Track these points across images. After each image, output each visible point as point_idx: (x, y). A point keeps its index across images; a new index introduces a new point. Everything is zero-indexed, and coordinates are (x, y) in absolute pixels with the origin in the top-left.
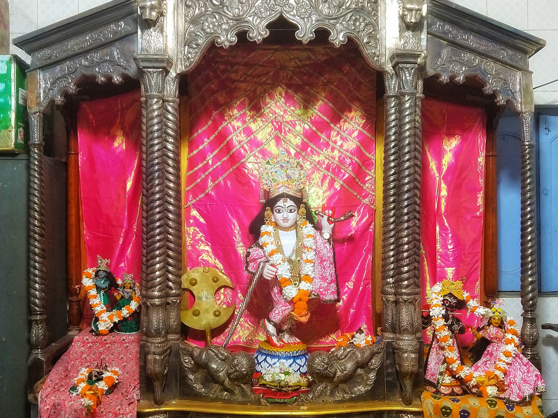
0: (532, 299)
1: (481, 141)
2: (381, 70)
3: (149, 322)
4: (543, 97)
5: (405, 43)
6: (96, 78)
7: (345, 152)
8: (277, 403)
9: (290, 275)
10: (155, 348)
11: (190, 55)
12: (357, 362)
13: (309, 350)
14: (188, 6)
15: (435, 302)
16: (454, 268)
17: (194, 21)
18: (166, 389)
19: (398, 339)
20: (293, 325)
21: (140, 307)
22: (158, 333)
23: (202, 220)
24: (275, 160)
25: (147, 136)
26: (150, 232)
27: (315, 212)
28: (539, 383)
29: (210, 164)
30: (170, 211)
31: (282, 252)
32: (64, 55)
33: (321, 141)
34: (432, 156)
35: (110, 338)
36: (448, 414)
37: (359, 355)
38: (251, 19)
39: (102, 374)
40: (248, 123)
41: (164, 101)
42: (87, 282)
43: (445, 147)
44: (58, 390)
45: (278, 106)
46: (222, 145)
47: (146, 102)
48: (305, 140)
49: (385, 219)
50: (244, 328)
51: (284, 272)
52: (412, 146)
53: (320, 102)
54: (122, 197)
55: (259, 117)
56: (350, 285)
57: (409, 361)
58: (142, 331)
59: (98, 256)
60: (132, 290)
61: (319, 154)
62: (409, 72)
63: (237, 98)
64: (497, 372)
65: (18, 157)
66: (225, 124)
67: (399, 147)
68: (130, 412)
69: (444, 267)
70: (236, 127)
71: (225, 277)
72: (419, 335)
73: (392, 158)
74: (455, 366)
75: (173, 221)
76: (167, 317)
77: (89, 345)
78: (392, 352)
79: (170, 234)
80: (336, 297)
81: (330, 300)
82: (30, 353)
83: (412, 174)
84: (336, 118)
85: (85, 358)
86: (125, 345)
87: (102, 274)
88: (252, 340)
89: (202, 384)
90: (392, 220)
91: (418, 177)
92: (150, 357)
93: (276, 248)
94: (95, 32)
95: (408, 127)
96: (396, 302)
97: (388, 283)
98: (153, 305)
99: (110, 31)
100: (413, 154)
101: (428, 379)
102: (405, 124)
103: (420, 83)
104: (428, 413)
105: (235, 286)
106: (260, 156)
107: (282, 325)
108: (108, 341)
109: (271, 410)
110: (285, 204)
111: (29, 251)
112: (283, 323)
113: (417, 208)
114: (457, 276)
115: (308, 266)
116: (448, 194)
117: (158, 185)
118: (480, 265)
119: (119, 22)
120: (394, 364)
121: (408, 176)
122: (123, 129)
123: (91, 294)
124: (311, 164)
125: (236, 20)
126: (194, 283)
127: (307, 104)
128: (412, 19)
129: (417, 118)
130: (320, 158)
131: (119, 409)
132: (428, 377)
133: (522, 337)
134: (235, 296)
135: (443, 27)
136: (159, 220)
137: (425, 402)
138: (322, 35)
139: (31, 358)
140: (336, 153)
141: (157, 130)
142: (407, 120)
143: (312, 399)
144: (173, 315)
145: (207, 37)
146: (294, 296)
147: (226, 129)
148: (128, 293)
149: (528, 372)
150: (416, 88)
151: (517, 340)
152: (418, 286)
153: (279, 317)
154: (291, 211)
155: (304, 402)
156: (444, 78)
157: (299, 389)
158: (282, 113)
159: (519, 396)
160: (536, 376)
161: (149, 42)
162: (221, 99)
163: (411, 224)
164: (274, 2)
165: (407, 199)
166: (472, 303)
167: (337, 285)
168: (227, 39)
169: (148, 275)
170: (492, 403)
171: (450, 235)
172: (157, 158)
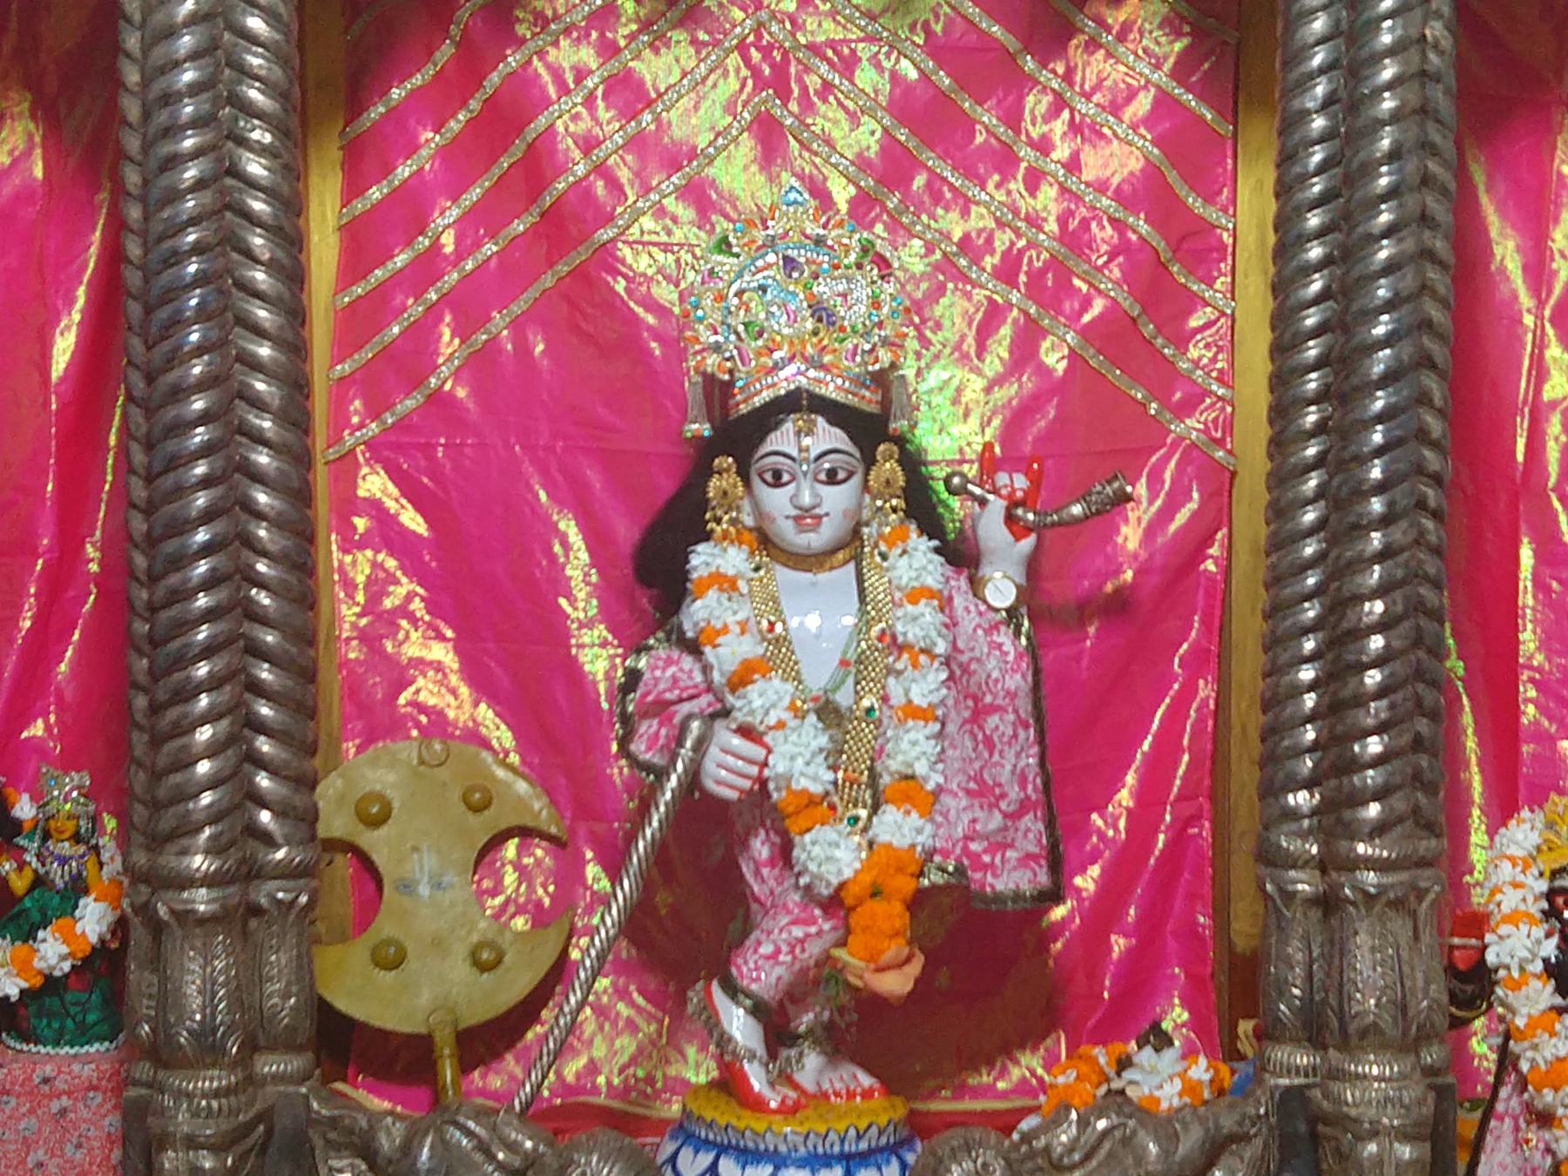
3: (168, 998)
9: (829, 776)
10: (195, 1114)
13: (919, 1127)
15: (1510, 900)
20: (841, 1010)
22: (208, 1049)
23: (412, 520)
25: (146, 115)
30: (258, 477)
33: (979, 139)
48: (902, 135)
49: (1280, 511)
50: (614, 1024)
51: (800, 761)
55: (680, 23)
58: (134, 1042)
60: (82, 849)
66: (513, 60)
67: (1349, 171)
69: (1553, 740)
70: (570, 78)
71: (522, 786)
73: (1314, 220)
75: (277, 523)
80: (1043, 878)
81: (1017, 896)
83: (1408, 299)
86: (55, 1106)
90: (1310, 516)
91: (1436, 314)
96: (1328, 903)
97: (1293, 814)
98: (185, 917)
102: (1376, 59)
105: (572, 831)
107: (791, 1009)
110: (807, 441)
115: (912, 735)
117: (199, 350)
122: (32, 84)
124: (930, 249)
126: (375, 814)
129: (1435, 30)
134: (568, 876)
136: (207, 517)
141: (195, 89)
146: (848, 873)
147: (522, 80)
148: (63, 861)
152: (1430, 828)
153: (779, 971)
154: (832, 478)
163: (1399, 533)
165: (1380, 418)
167: (1050, 825)
169: (157, 776)
172: (193, 221)
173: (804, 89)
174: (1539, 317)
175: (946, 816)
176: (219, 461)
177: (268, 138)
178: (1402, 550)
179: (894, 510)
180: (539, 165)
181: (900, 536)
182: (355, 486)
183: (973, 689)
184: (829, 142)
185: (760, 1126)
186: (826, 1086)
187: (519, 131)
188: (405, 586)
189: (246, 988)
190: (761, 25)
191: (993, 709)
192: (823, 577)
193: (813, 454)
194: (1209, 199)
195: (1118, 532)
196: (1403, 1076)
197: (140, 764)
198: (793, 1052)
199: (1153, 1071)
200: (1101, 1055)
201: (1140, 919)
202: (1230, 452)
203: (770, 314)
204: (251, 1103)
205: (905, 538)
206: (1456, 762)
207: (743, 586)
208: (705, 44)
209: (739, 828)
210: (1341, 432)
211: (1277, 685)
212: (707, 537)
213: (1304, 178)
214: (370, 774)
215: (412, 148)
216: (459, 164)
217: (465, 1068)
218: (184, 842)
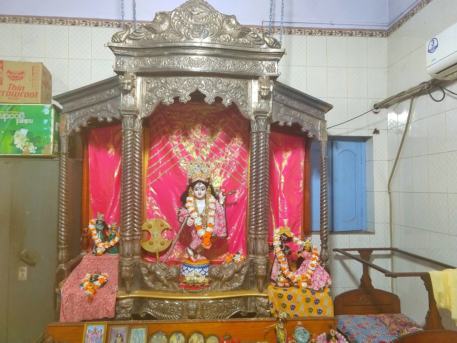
0: (326, 237)
1: (302, 154)
3: (124, 249)
4: (333, 132)
12: (235, 271)
13: (211, 263)
14: (148, 83)
15: (276, 238)
17: (151, 90)
19: (256, 258)
22: (128, 255)
23: (155, 193)
25: (124, 150)
28: (329, 280)
30: (136, 190)
31: (198, 212)
32: (81, 106)
35: (104, 257)
36: (281, 297)
38: (181, 91)
41: (134, 132)
42: (91, 227)
44: (73, 286)
45: (197, 134)
47: (125, 132)
48: (212, 152)
49: (251, 195)
52: (264, 158)
53: (220, 132)
54: (112, 180)
55: (187, 139)
56: (234, 228)
57: (261, 270)
63: (176, 129)
64: (307, 275)
65: (54, 159)
66: (169, 142)
71: (167, 224)
72: (267, 256)
73: (254, 164)
74: (286, 272)
76: (133, 247)
78: (253, 265)
81: (223, 237)
82: (58, 266)
84: (228, 141)
88: (181, 258)
89: (152, 282)
90: (254, 195)
91: (267, 174)
92: (123, 268)
96: (255, 239)
97: (252, 229)
100: (264, 162)
103: (269, 126)
109: (188, 296)
111: (59, 210)
113: (267, 190)
117: (129, 176)
118: (301, 218)
121: (262, 173)
122: (114, 144)
124: (215, 164)
126: (150, 227)
127: (213, 133)
128: (264, 94)
129: (267, 144)
130: (219, 162)
132: (272, 278)
133: (320, 257)
135: (281, 97)
136: (130, 195)
138: (218, 100)
139: (58, 269)
140: (228, 159)
141: (130, 147)
142: (261, 145)
144: (137, 245)
147: (169, 145)
149: (323, 275)
150: (266, 129)
151: (318, 258)
154: (203, 190)
156: (281, 123)
159: (318, 287)
160: (327, 277)
161: (128, 101)
163: (263, 198)
165: (261, 185)
166: (295, 239)
167: (227, 229)
168: (169, 101)
169: (123, 224)
170: (304, 292)
172: (129, 162)
180: (171, 154)
188: (154, 201)
191: (220, 216)
194: (245, 159)
206: (272, 221)
212: (189, 196)
215: (156, 152)
216: (162, 154)
217: (160, 256)
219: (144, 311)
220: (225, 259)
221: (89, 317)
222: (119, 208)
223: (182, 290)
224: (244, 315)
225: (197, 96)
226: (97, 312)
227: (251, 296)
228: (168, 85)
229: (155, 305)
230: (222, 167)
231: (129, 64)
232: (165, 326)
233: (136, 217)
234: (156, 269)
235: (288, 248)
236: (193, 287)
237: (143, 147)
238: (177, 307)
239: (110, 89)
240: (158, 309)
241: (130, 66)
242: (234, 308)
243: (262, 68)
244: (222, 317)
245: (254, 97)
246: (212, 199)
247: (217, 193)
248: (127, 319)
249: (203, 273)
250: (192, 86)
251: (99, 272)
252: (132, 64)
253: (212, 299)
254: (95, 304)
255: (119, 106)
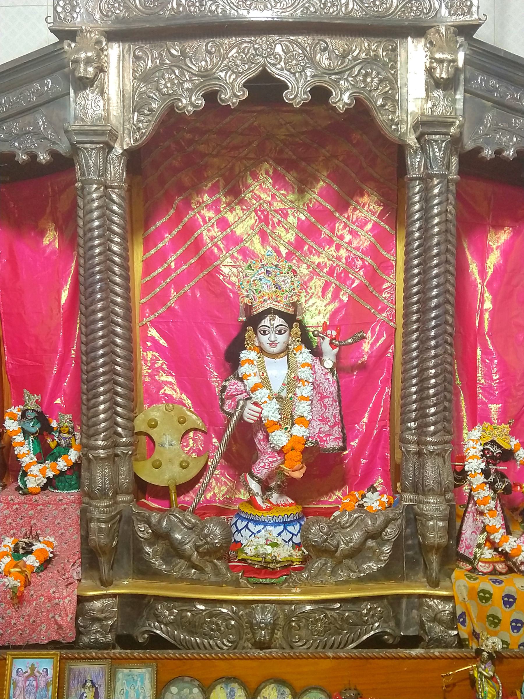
2: (400, 143)
3: (92, 480)
5: (433, 106)
6: (15, 156)
7: (354, 252)
8: (261, 583)
9: (280, 416)
10: (100, 513)
11: (140, 125)
13: (306, 513)
14: (137, 58)
15: (472, 452)
16: (500, 405)
17: (146, 78)
18: (115, 565)
19: (421, 502)
20: (283, 482)
21: (80, 458)
22: (103, 494)
23: (162, 342)
24: (260, 264)
25: (85, 234)
26: (91, 362)
27: (313, 332)
29: (173, 267)
30: (117, 335)
31: (269, 387)
33: (323, 236)
34: (472, 256)
35: (43, 497)
36: (487, 600)
37: (370, 523)
38: (222, 75)
39: (33, 545)
40: (222, 213)
42: (11, 425)
43: (490, 243)
45: (262, 189)
46: (189, 243)
47: (83, 188)
48: (301, 235)
49: (406, 344)
50: (221, 483)
51: (271, 412)
52: (443, 247)
53: (322, 183)
55: (238, 204)
57: (435, 530)
58: (83, 491)
59: (25, 391)
60: (70, 436)
61: (319, 254)
62: (438, 147)
63: (207, 179)
66: (191, 214)
67: (425, 248)
68: (69, 596)
69: (486, 404)
70: (207, 219)
71: (194, 417)
72: (449, 496)
73: (416, 262)
74: (497, 537)
75: (122, 347)
77: (15, 507)
78: (413, 518)
79: (118, 365)
80: (341, 444)
81: (333, 449)
83: (442, 285)
84: (343, 206)
85: (10, 523)
86: (63, 507)
87: (31, 414)
88: (230, 498)
89: (162, 559)
90: (415, 345)
91: (450, 288)
92: (93, 525)
93: (260, 381)
94: (14, 93)
95: (436, 220)
96: (419, 454)
97: (409, 429)
98: (97, 458)
99: (33, 92)
100: (443, 257)
101: (462, 552)
102: (433, 217)
103: (454, 160)
104: (461, 599)
105: (208, 429)
106: (240, 258)
107: (269, 481)
108: (40, 502)
109: (253, 593)
110: (272, 322)
112: (270, 479)
113: (449, 329)
114: (503, 418)
115: (303, 405)
116: (493, 306)
117: (100, 300)
119: (45, 79)
120: (415, 534)
121: (437, 287)
122: (55, 221)
123: (16, 441)
124: (309, 267)
125: (202, 77)
126: (153, 425)
127: (303, 186)
128: (442, 73)
129: (450, 208)
130: (321, 260)
131: (54, 592)
132: (462, 550)
134: (208, 442)
135: (486, 82)
137: (457, 584)
138: (320, 94)
140: (343, 253)
141: (98, 227)
142: (435, 211)
143: (307, 578)
144: (124, 470)
145: (164, 100)
146: (285, 444)
147: (193, 220)
148: (65, 439)
150: (448, 168)
152: (449, 433)
153: (265, 471)
154: (280, 333)
155: (297, 583)
156: (488, 153)
157: (290, 565)
158: (269, 199)
161: (90, 107)
162: (186, 179)
163: (439, 350)
164: (254, 52)
165: (434, 318)
167: (343, 429)
168: (191, 102)
169: (89, 419)
171: (496, 361)
172: (98, 264)
173: (273, 222)
174: (483, 285)
175: (313, 428)
176: (106, 331)
177: (119, 240)
178: (441, 355)
179: (298, 341)
180: (198, 243)
181: (299, 349)
182: (147, 333)
183: (321, 391)
184: (280, 237)
185: (260, 515)
186: (279, 503)
187: (193, 234)
188: (160, 362)
189: (115, 475)
190: (261, 204)
192: (278, 360)
193: (275, 326)
194: (389, 252)
195: (362, 345)
196: (440, 503)
197: (85, 415)
198: (270, 493)
199: (371, 499)
200: (357, 494)
201: (369, 455)
202: (395, 323)
203: (262, 287)
204: (116, 509)
205: (301, 349)
207: (255, 363)
208: (245, 210)
209: (254, 430)
210: (423, 321)
211: (405, 392)
212: (245, 349)
213: (413, 250)
214: (152, 413)
215: (163, 239)
216: (175, 244)
217: (178, 495)
218: (97, 437)
219: (144, 629)
220: (339, 503)
221: (15, 639)
222: (77, 379)
223: (237, 579)
224: (391, 641)
225: (265, 89)
226: (34, 627)
227: (409, 596)
228: (188, 61)
229: (171, 614)
230: (328, 273)
231: (87, 10)
232: (198, 663)
233: (119, 399)
234: (172, 526)
235: (502, 476)
236: (264, 571)
237: (128, 227)
238: (225, 620)
239: (41, 77)
240: (179, 623)
241: (90, 14)
242: (366, 623)
243: (437, 5)
244: (336, 645)
245: (415, 85)
246: (305, 355)
247: (316, 340)
248: (106, 646)
249: (286, 536)
250: (250, 61)
251: (34, 534)
252: (94, 8)
253: (311, 602)
254: (29, 610)
255: (65, 120)
